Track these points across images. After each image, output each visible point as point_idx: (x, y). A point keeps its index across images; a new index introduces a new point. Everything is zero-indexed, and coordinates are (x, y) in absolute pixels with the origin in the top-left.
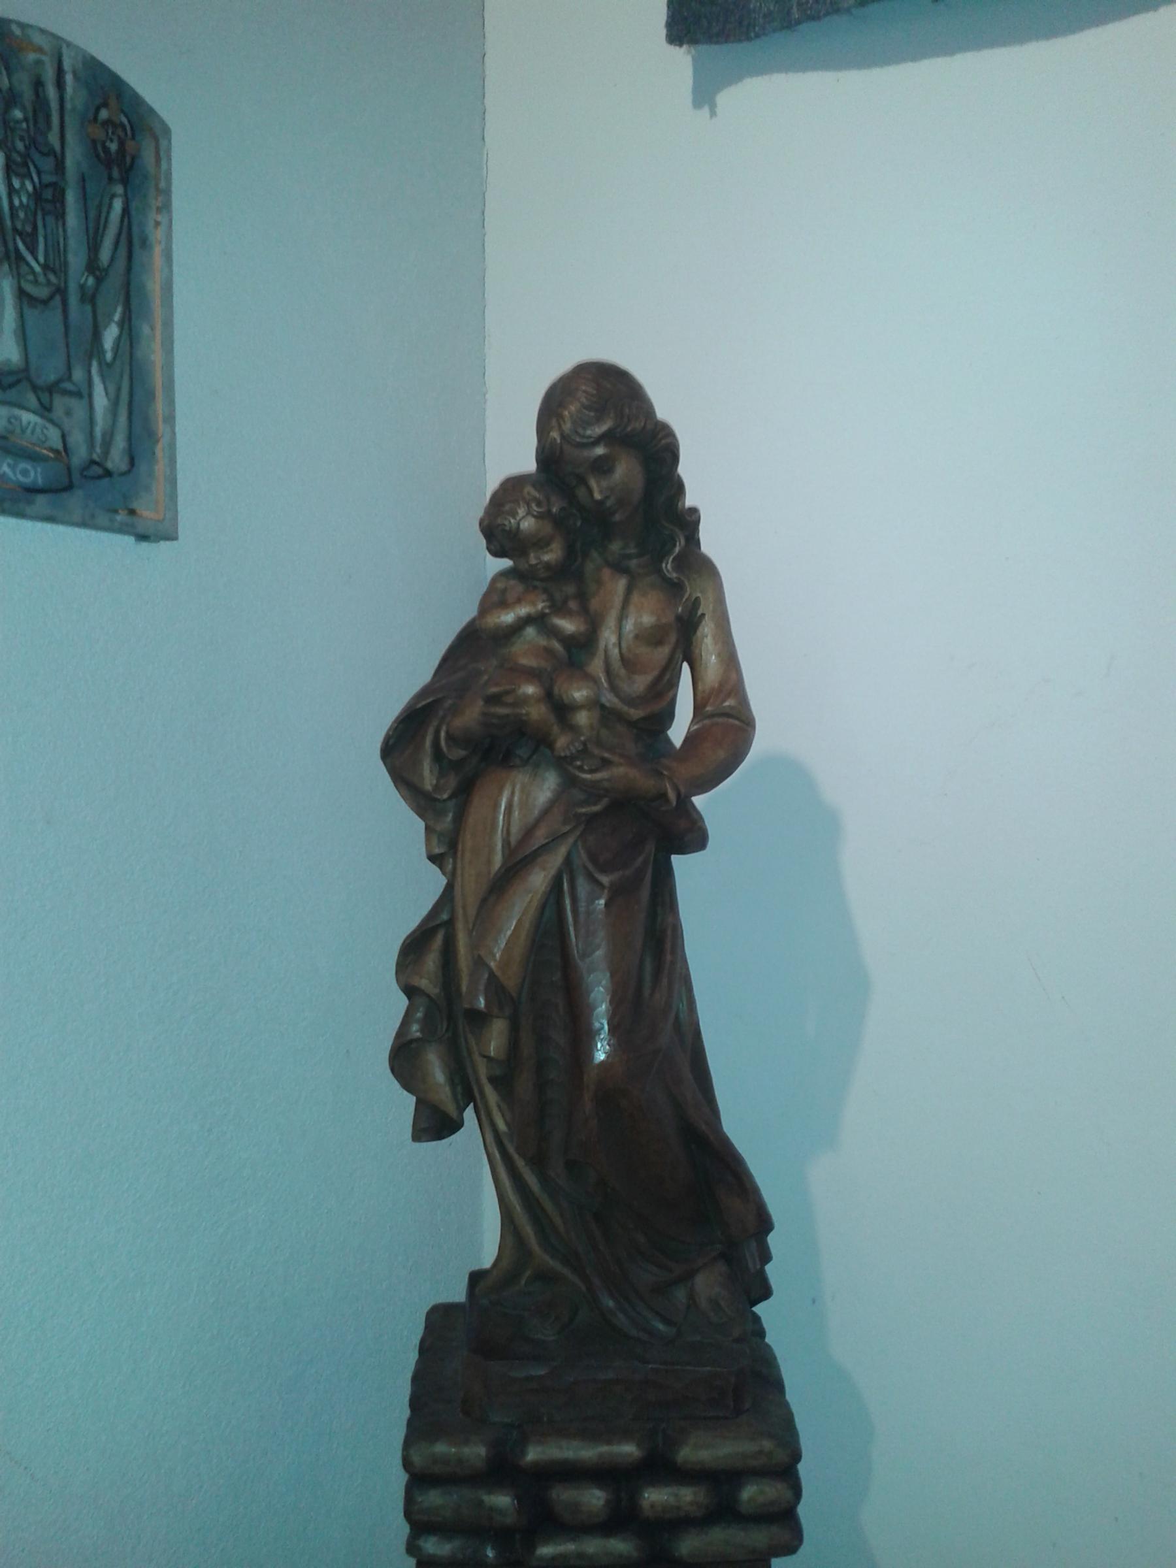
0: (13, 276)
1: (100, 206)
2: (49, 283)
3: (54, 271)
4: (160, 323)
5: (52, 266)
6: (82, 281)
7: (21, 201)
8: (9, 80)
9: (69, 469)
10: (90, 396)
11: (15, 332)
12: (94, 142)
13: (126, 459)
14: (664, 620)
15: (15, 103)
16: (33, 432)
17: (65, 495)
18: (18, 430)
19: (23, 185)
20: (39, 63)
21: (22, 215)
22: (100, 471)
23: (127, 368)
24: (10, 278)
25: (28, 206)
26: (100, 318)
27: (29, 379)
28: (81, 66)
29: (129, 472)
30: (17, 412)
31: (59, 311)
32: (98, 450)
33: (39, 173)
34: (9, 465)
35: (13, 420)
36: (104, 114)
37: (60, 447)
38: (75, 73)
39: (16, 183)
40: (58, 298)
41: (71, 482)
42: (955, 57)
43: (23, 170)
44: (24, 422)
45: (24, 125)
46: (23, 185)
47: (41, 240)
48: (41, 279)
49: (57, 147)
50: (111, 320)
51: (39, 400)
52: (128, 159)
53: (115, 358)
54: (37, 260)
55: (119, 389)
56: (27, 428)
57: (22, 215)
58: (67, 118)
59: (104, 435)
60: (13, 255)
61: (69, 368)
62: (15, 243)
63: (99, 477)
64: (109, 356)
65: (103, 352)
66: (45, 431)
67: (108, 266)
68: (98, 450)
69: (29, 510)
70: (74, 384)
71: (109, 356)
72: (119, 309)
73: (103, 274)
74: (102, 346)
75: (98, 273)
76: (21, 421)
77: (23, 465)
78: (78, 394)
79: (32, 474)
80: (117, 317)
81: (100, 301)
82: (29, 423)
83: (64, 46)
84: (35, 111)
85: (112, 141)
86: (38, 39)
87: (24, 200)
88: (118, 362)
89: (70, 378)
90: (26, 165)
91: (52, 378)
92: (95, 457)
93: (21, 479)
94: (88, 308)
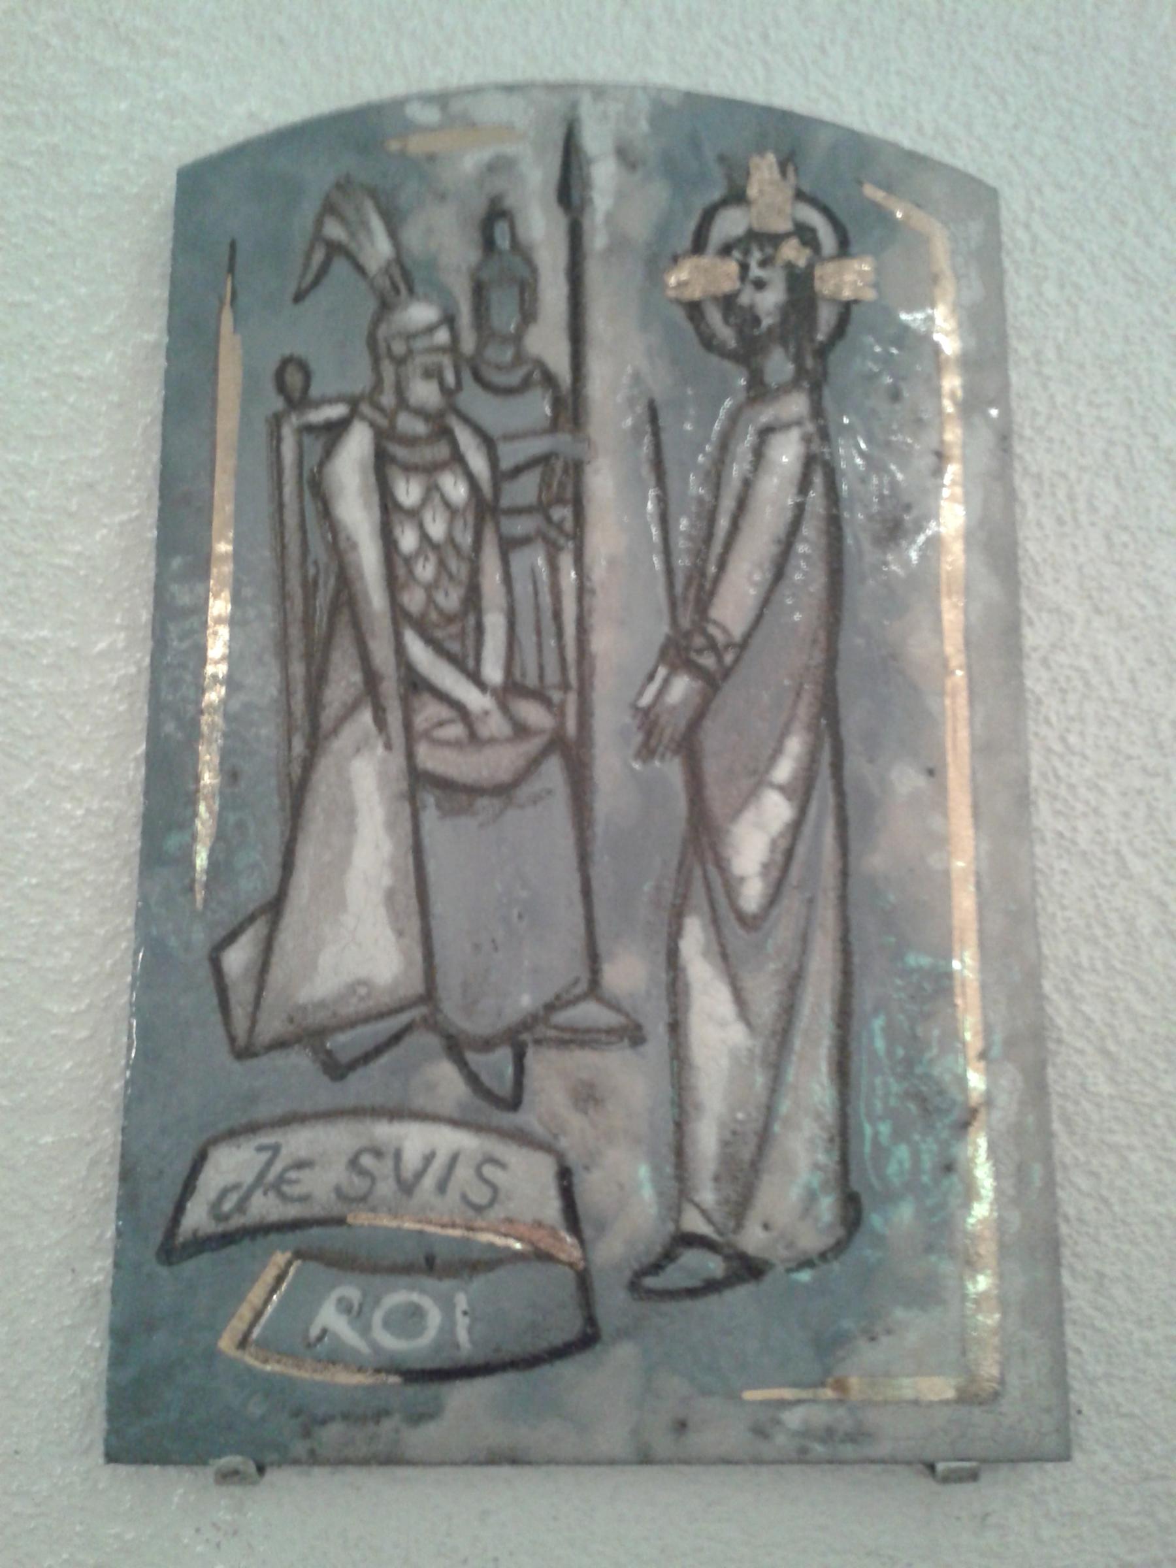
0: (388, 746)
1: (716, 478)
2: (521, 730)
3: (539, 695)
4: (965, 746)
5: (532, 680)
6: (646, 700)
7: (424, 537)
8: (393, 234)
9: (584, 1281)
10: (676, 1028)
11: (390, 896)
12: (694, 310)
13: (827, 1206)
14: (231, 535)
15: (411, 291)
16: (442, 1187)
17: (566, 1369)
18: (386, 1188)
19: (432, 489)
20: (499, 166)
21: (426, 570)
22: (715, 1266)
23: (827, 915)
24: (380, 750)
25: (451, 539)
26: (714, 793)
27: (432, 1024)
28: (644, 126)
29: (839, 1248)
30: (384, 1131)
31: (559, 808)
32: (707, 1196)
33: (488, 443)
34: (345, 1307)
35: (367, 1161)
36: (730, 223)
37: (552, 1209)
38: (625, 155)
39: (408, 492)
40: (553, 771)
41: (591, 1320)
42: (411, 851)
43: (442, 451)
44: (412, 1158)
45: (442, 336)
46: (432, 489)
47: (495, 623)
48: (496, 725)
49: (558, 360)
50: (760, 780)
51: (473, 1079)
52: (826, 317)
53: (774, 896)
54: (476, 678)
55: (789, 1010)
56: (420, 1175)
57: (426, 570)
58: (594, 272)
59: (728, 1159)
60: (390, 687)
61: (594, 959)
62: (400, 650)
63: (711, 1286)
64: (752, 894)
65: (731, 886)
66: (489, 1171)
67: (748, 636)
68: (707, 1196)
69: (419, 1438)
70: (614, 1006)
71: (752, 894)
72: (795, 745)
73: (729, 658)
74: (722, 865)
75: (708, 661)
76: (398, 1155)
77: (399, 1296)
78: (634, 1035)
79: (434, 1318)
80: (784, 771)
81: (712, 737)
82: (429, 1158)
83: (586, 99)
84: (479, 291)
85: (760, 285)
86: (493, 110)
87: (437, 529)
88: (792, 902)
89: (594, 988)
90: (446, 433)
91: (526, 1002)
92: (694, 1223)
93: (390, 1342)
94: (672, 770)
